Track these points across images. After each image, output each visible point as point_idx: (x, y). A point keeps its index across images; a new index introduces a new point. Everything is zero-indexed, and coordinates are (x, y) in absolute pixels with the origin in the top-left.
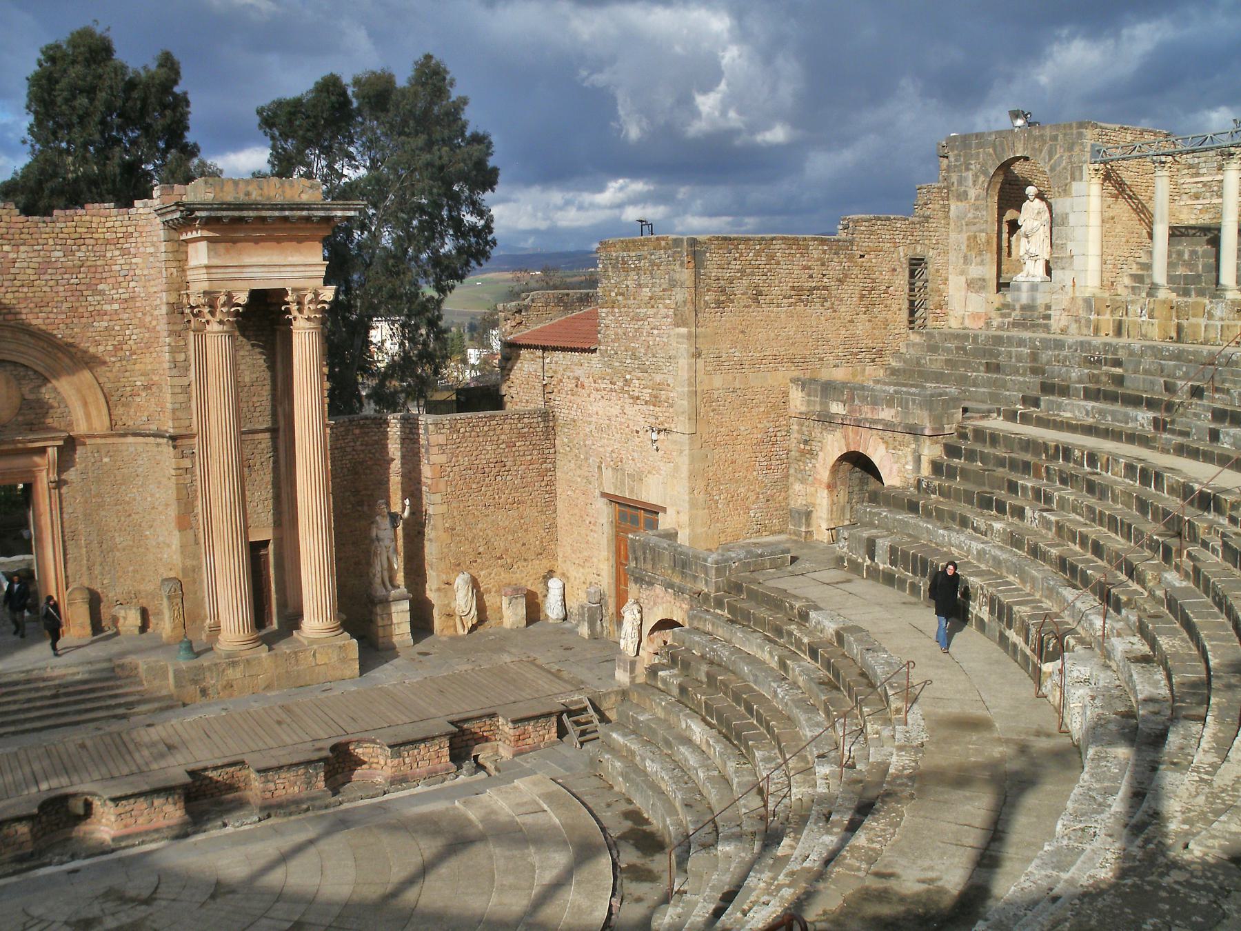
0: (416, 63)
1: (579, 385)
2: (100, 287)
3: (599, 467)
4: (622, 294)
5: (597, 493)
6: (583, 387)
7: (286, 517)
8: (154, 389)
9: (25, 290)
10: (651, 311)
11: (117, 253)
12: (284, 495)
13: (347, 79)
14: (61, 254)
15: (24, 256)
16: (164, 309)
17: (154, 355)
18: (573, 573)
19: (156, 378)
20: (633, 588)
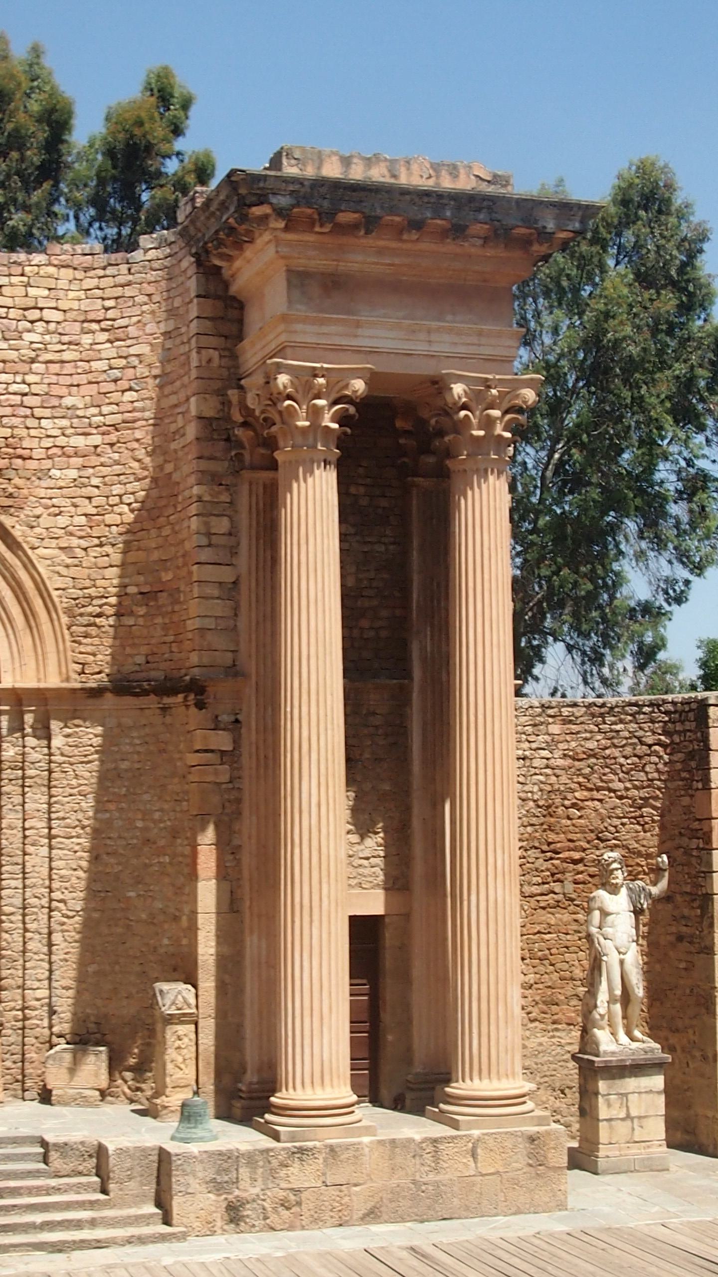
0: (620, 177)
2: (68, 401)
7: (419, 869)
8: (163, 598)
11: (104, 336)
12: (416, 824)
13: (111, 1148)
16: (192, 431)
17: (166, 531)
19: (167, 576)
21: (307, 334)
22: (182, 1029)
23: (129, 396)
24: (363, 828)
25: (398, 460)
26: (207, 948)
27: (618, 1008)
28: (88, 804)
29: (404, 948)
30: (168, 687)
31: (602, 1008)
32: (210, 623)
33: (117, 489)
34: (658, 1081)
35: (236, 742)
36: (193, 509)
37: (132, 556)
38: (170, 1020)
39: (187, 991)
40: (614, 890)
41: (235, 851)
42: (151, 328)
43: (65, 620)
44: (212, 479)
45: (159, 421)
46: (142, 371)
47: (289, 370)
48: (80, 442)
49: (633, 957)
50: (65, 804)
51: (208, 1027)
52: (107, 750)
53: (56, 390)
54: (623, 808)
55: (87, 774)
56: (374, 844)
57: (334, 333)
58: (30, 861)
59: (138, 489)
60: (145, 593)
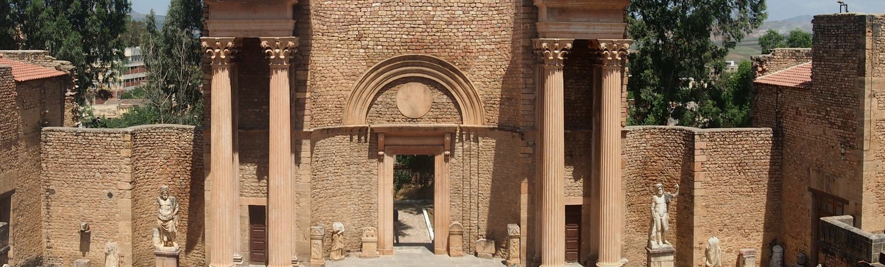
1: (798, 113)
2: (484, 34)
3: (808, 170)
4: (826, 52)
5: (806, 188)
6: (801, 115)
9: (439, 34)
10: (844, 65)
11: (495, 12)
12: (593, 177)
14: (461, 12)
15: (440, 13)
18: (790, 242)
20: (822, 256)
21: (553, 28)
22: (515, 240)
23: (504, 33)
24: (576, 179)
25: (584, 66)
26: (524, 215)
27: (660, 234)
28: (491, 164)
29: (588, 215)
30: (514, 130)
31: (654, 234)
32: (526, 113)
33: (500, 63)
34: (672, 257)
35: (534, 151)
36: (521, 75)
37: (505, 86)
38: (512, 237)
39: (516, 227)
40: (660, 196)
41: (533, 185)
42: (510, 11)
43: (483, 105)
44: (527, 66)
45: (513, 42)
46: (507, 25)
47: (546, 41)
48: (488, 47)
49: (665, 217)
50: (483, 163)
51: (524, 240)
52: (497, 148)
53: (481, 30)
54: (670, 163)
55: (491, 154)
56: (580, 183)
57: (562, 27)
58: (472, 181)
59: (506, 64)
60: (508, 99)
